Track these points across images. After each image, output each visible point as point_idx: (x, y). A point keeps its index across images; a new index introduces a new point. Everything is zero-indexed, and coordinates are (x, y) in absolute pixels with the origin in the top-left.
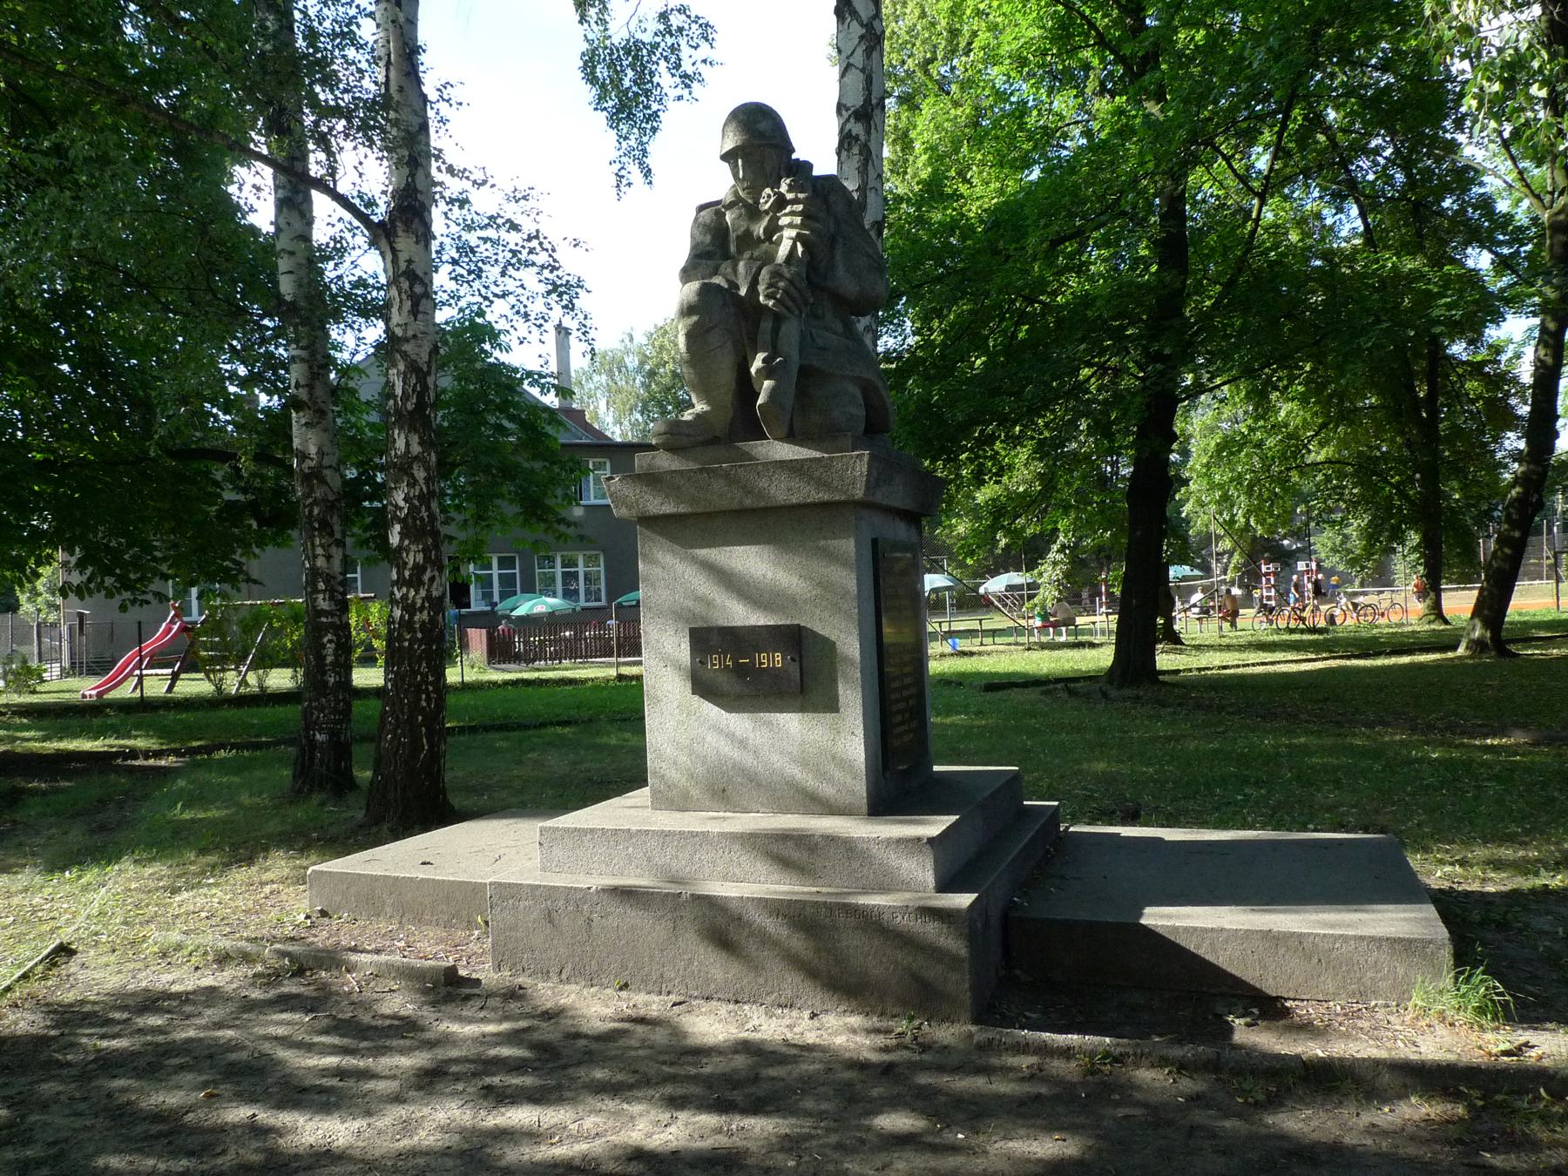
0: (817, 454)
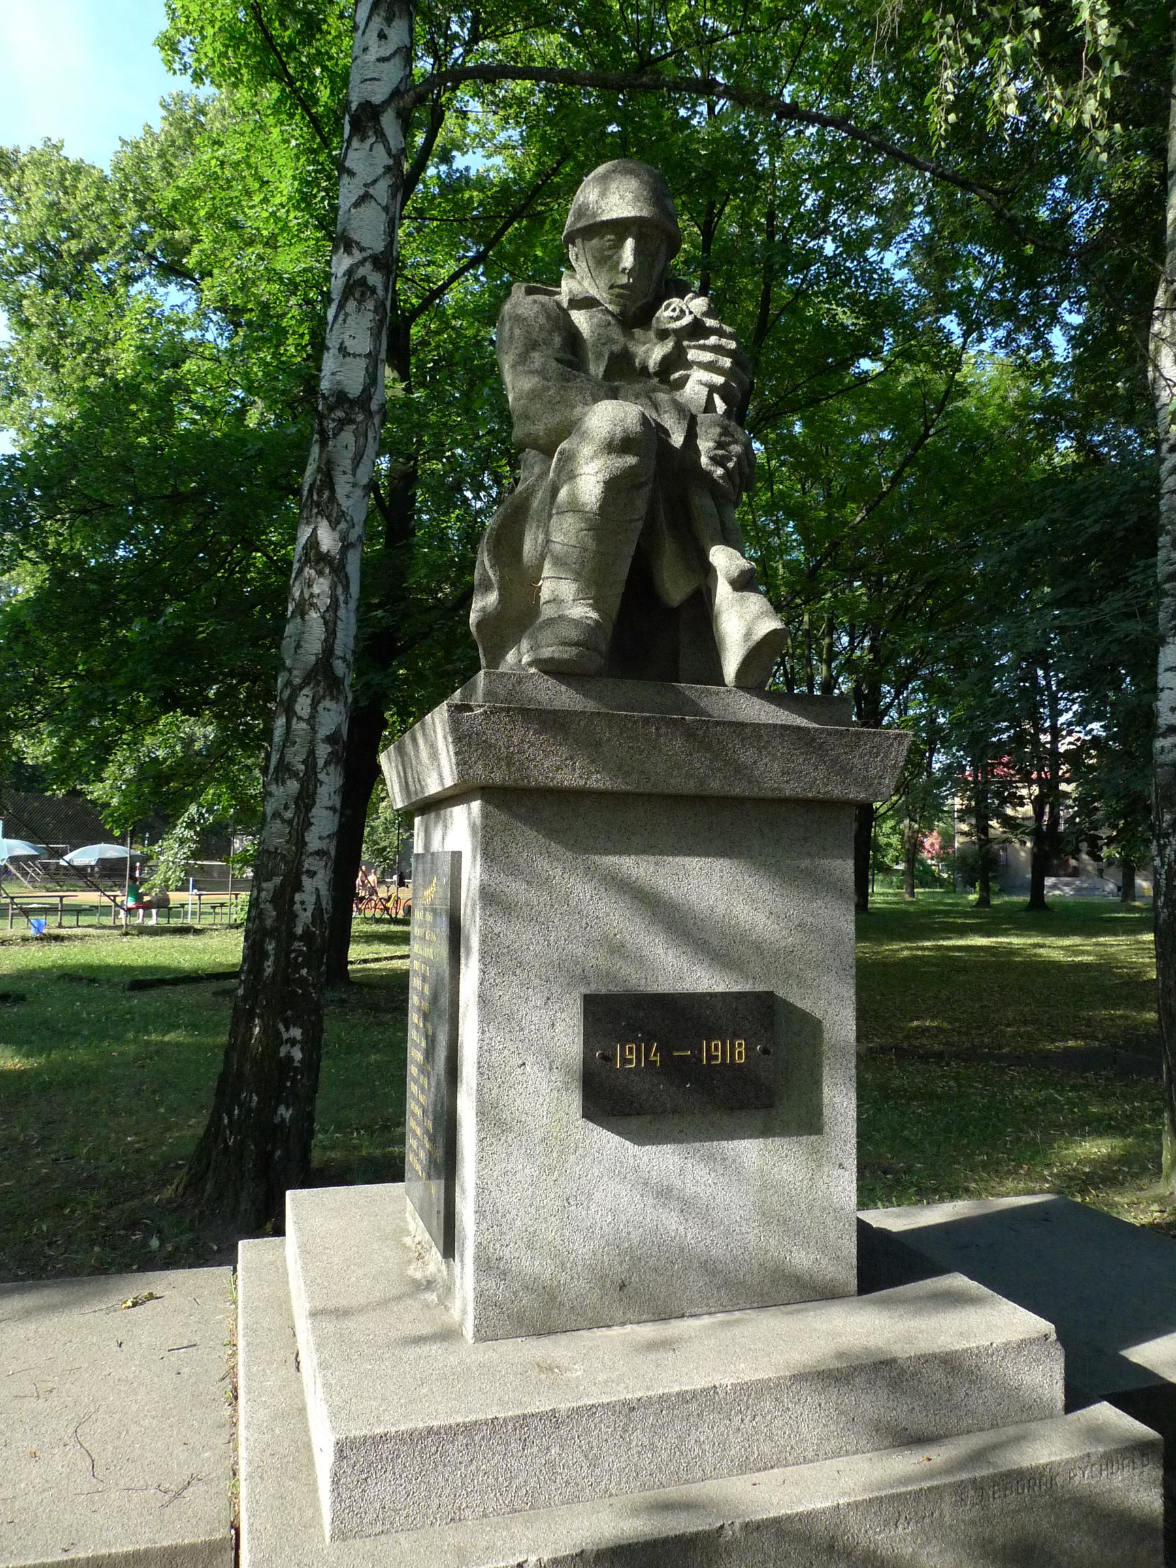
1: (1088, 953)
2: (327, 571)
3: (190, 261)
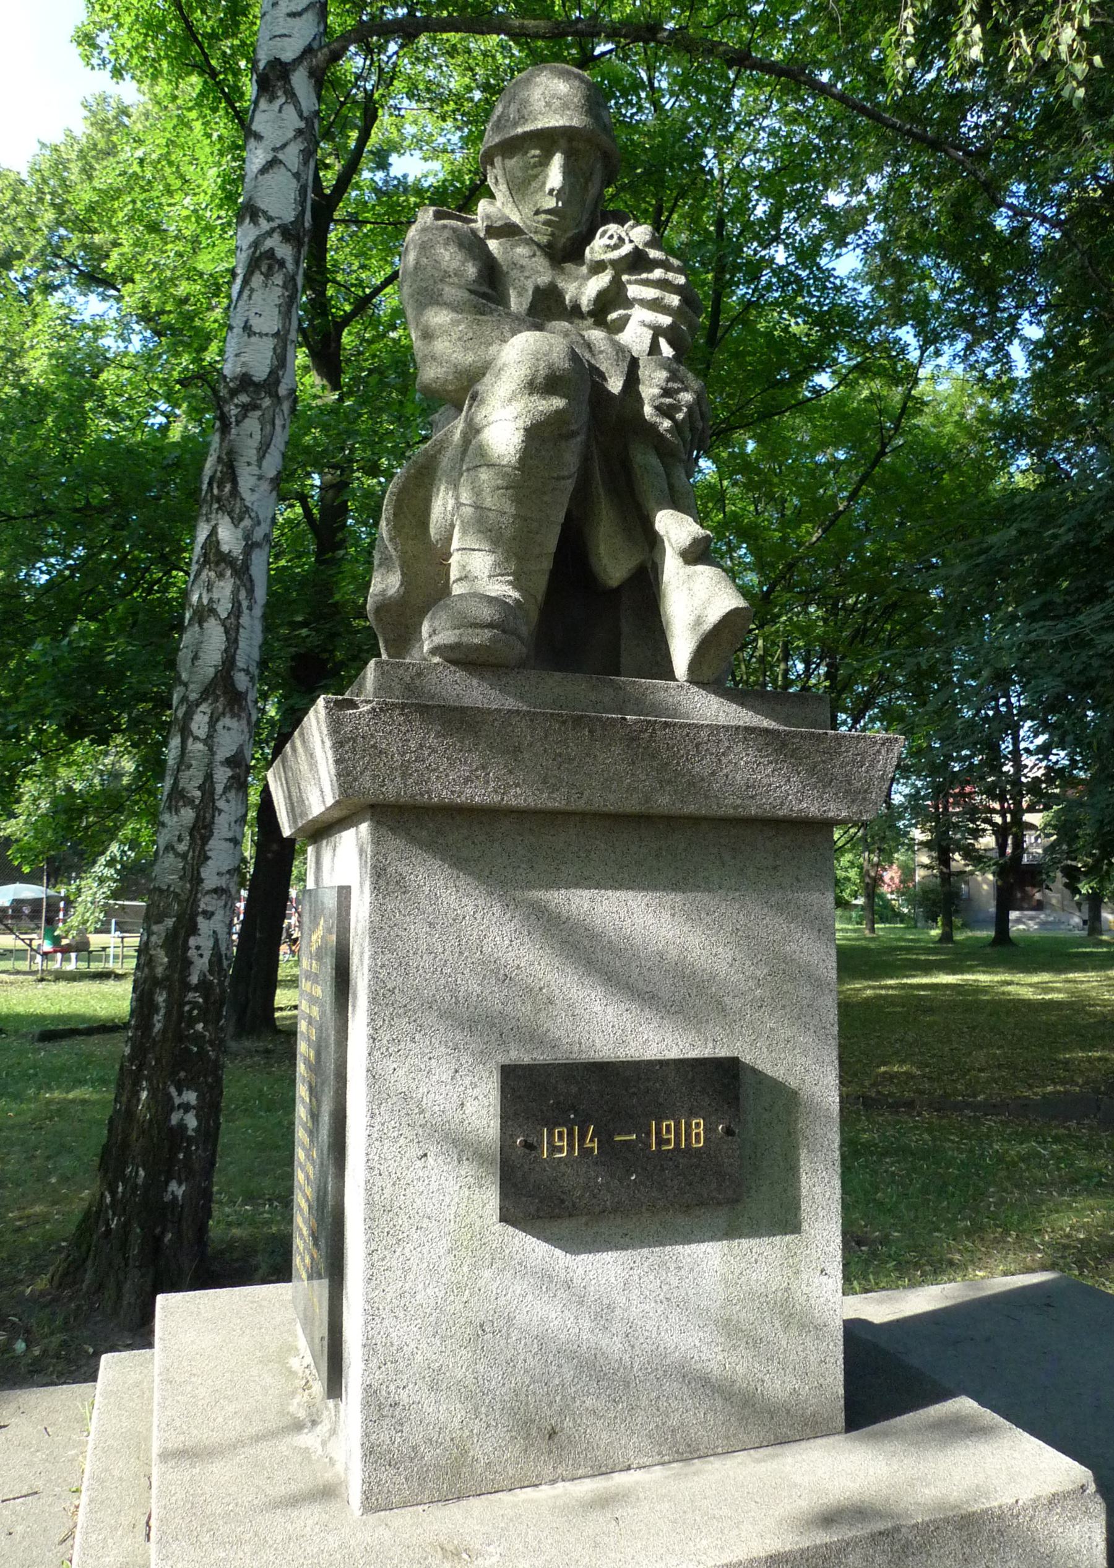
0: (766, 723)
1: (1059, 990)
2: (229, 573)
3: (109, 266)
